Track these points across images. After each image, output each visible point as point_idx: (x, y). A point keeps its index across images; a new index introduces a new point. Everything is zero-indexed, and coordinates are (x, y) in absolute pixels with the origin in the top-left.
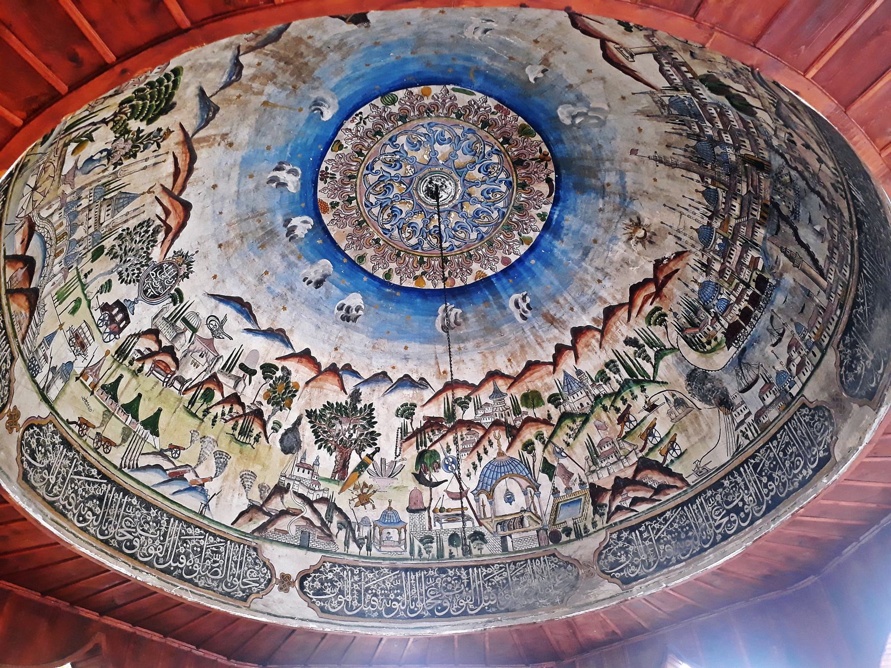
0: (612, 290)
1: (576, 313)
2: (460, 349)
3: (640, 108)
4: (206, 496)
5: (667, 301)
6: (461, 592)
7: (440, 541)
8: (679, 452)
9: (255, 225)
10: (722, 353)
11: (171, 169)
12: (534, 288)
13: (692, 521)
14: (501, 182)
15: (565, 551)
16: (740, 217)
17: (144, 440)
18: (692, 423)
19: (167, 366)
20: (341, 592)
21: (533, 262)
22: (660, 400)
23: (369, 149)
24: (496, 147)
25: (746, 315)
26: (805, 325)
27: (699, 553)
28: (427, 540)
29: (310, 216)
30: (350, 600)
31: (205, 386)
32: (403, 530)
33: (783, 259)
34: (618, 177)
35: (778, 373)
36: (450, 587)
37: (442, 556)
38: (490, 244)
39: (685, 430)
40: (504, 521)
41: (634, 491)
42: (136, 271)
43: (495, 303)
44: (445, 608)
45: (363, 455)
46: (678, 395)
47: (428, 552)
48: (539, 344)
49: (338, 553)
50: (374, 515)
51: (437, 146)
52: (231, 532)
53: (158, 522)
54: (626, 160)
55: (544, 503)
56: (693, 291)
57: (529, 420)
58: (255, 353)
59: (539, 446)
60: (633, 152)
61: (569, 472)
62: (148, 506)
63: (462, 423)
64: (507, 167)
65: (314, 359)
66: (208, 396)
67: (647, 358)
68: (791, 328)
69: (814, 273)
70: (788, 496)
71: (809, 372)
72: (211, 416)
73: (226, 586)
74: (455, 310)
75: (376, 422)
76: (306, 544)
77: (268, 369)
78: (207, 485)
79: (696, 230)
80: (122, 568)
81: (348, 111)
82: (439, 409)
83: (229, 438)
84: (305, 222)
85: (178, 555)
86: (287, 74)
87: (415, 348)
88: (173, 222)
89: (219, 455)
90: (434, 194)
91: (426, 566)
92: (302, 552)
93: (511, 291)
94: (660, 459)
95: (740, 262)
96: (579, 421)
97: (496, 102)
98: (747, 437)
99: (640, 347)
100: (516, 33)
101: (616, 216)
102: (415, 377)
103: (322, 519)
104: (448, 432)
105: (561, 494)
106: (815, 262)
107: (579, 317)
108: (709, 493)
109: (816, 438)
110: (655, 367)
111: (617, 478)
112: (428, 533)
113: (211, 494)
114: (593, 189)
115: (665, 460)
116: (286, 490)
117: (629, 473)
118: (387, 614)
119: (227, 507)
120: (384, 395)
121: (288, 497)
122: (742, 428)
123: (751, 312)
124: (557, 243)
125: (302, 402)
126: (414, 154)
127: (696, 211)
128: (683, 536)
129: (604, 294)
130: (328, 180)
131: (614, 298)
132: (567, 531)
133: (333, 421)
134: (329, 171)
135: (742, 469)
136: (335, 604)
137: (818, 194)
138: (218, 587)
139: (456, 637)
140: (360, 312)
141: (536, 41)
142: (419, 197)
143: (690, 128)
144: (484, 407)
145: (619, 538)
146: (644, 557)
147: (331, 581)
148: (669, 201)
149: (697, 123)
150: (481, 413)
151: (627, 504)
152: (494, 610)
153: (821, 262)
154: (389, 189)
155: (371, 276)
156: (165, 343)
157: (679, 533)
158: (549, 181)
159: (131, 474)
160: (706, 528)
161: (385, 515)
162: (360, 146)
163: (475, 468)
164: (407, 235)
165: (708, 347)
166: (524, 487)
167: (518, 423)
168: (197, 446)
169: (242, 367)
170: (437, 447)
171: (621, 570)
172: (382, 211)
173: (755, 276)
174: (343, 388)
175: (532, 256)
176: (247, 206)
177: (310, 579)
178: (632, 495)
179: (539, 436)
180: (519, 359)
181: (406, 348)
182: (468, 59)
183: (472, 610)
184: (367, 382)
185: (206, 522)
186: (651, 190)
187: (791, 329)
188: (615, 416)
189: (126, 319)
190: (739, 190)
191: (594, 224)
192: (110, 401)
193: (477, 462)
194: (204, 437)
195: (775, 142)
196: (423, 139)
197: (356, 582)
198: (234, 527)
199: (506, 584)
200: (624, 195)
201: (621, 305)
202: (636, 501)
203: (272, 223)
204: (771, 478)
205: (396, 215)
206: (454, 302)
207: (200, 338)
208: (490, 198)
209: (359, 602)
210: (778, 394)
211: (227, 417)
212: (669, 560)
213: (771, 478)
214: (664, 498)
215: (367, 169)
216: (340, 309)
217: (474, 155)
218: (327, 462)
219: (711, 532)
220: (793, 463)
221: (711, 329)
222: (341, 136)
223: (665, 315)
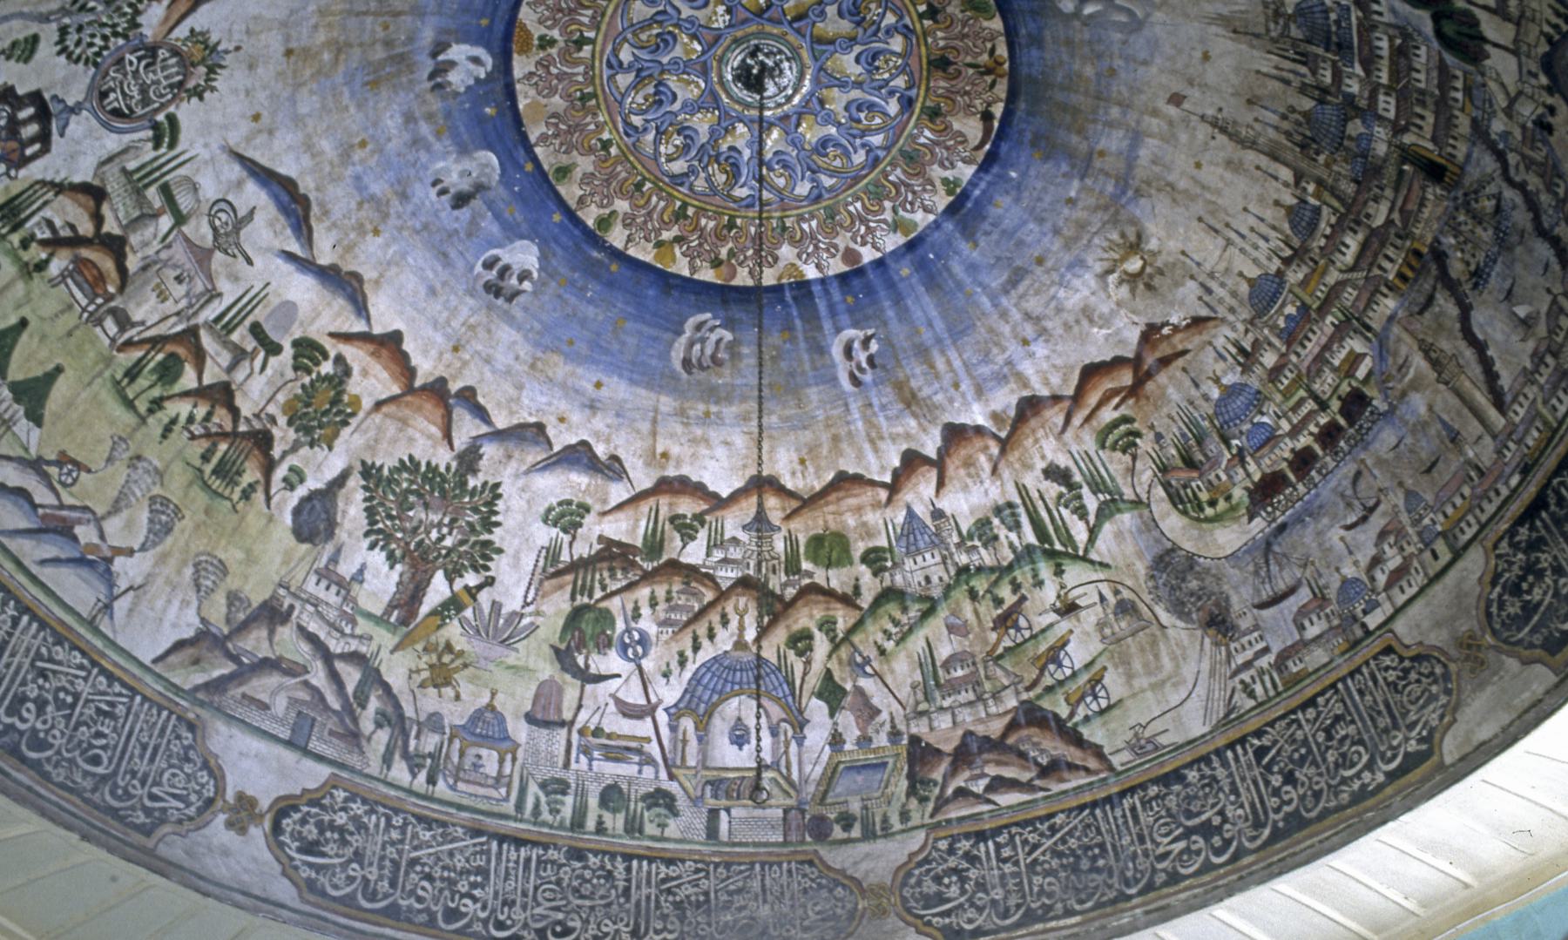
0: (1045, 366)
1: (963, 395)
2: (707, 414)
3: (1225, 11)
5: (1149, 408)
6: (609, 905)
7: (582, 794)
8: (1104, 703)
13: (1108, 839)
14: (891, 93)
15: (837, 858)
16: (1353, 269)
18: (1142, 650)
19: (101, 278)
20: (358, 856)
21: (905, 272)
24: (907, 21)
25: (1303, 461)
26: (1429, 497)
27: (1114, 902)
30: (372, 878)
31: (170, 348)
33: (1419, 362)
34: (1125, 143)
35: (1345, 582)
38: (832, 214)
40: (722, 781)
41: (999, 763)
42: (98, 41)
43: (806, 339)
45: (459, 584)
46: (1126, 594)
47: (554, 812)
48: (872, 442)
49: (368, 776)
50: (455, 715)
52: (149, 679)
54: (1155, 113)
56: (1206, 398)
58: (289, 308)
59: (821, 645)
60: (1176, 99)
63: (674, 566)
64: (915, 66)
65: (405, 357)
66: (169, 371)
67: (1081, 512)
68: (1399, 499)
69: (1481, 399)
70: (1320, 818)
71: (1415, 589)
72: (164, 416)
73: (113, 793)
75: (498, 524)
77: (308, 350)
78: (119, 563)
79: (1250, 281)
83: (190, 474)
84: (476, 60)
85: (21, 699)
87: (618, 389)
89: (159, 504)
90: (753, 80)
92: (289, 756)
93: (844, 319)
94: (1064, 711)
95: (1320, 360)
96: (914, 611)
98: (1252, 695)
99: (1071, 486)
101: (1097, 220)
102: (600, 450)
105: (848, 747)
106: (1491, 377)
107: (966, 404)
108: (1153, 790)
109: (1405, 715)
110: (1093, 533)
112: (560, 774)
113: (123, 584)
114: (1070, 155)
115: (1072, 715)
116: (285, 618)
117: (995, 728)
119: (155, 623)
120: (527, 472)
121: (286, 633)
122: (1246, 676)
123: (1314, 457)
124: (964, 247)
125: (359, 440)
127: (1261, 243)
128: (1085, 864)
129: (1027, 368)
131: (1046, 383)
132: (847, 821)
133: (412, 498)
135: (1229, 754)
136: (340, 878)
138: (94, 790)
140: (527, 285)
142: (721, 77)
143: (1314, 73)
145: (951, 851)
146: (998, 894)
147: (341, 830)
148: (1212, 213)
149: (1334, 63)
150: (718, 555)
151: (979, 787)
153: (1505, 381)
154: (666, 42)
156: (111, 226)
157: (1078, 858)
158: (987, 117)
160: (1134, 857)
161: (477, 716)
163: (682, 663)
164: (671, 150)
165: (1209, 511)
167: (790, 592)
168: (120, 473)
169: (256, 330)
170: (615, 604)
171: (947, 914)
172: (635, 86)
173: (1345, 388)
174: (448, 436)
178: (992, 770)
179: (827, 625)
181: (598, 385)
184: (499, 435)
185: (99, 643)
186: (1183, 184)
187: (1394, 500)
188: (989, 612)
189: (44, 138)
190: (1368, 216)
191: (1048, 225)
193: (689, 653)
194: (139, 458)
195: (1498, 126)
197: (393, 843)
198: (158, 669)
200: (1127, 185)
201: (1056, 399)
202: (999, 784)
204: (1290, 779)
205: (660, 103)
206: (722, 313)
207: (187, 240)
209: (393, 884)
210: (1336, 622)
211: (197, 429)
212: (1049, 908)
213: (1290, 779)
214: (1056, 788)
216: (488, 265)
217: (858, 24)
218: (382, 580)
220: (1343, 755)
221: (1224, 477)
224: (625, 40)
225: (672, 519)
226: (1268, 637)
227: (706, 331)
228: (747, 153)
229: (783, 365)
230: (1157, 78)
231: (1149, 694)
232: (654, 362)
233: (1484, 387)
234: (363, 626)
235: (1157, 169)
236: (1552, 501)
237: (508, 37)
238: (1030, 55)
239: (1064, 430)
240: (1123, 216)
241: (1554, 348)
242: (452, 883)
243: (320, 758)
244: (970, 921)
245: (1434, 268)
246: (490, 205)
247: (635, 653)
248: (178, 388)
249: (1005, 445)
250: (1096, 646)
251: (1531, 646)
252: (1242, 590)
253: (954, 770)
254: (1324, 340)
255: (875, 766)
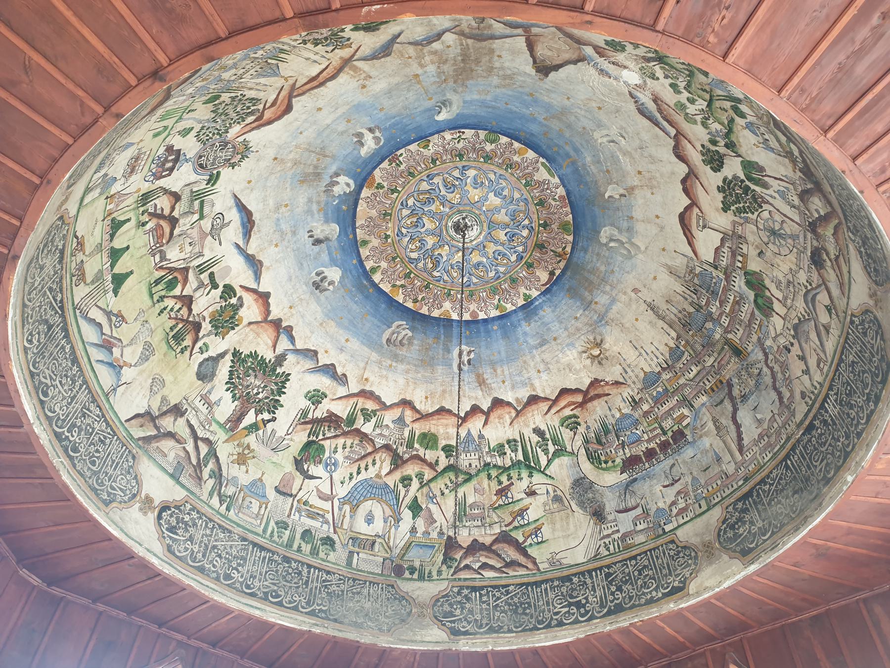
2: (391, 366)
3: (669, 264)
4: (119, 380)
7: (294, 531)
9: (313, 160)
10: (614, 474)
11: (314, 74)
12: (483, 349)
13: (532, 601)
14: (515, 252)
16: (691, 380)
17: (106, 292)
18: (562, 520)
19: (163, 235)
20: (191, 539)
21: (495, 328)
22: (541, 490)
23: (443, 162)
24: (533, 225)
25: (650, 454)
28: (282, 525)
29: (355, 182)
30: (196, 550)
31: (175, 274)
32: (264, 506)
33: (710, 425)
36: (289, 578)
37: (291, 546)
39: (553, 523)
41: (486, 557)
42: (211, 135)
43: (444, 344)
44: (280, 596)
45: (260, 417)
46: (559, 493)
49: (201, 500)
51: (491, 195)
52: (121, 429)
53: (74, 382)
54: (625, 293)
55: (400, 536)
56: (613, 416)
57: (417, 457)
58: (228, 269)
59: (415, 484)
60: (636, 291)
61: (433, 518)
62: (75, 361)
63: (358, 431)
66: (171, 285)
67: (546, 451)
68: (689, 479)
69: (734, 447)
70: (631, 608)
71: (689, 518)
72: (162, 305)
74: (408, 331)
75: (284, 393)
76: (177, 475)
77: (229, 290)
79: (645, 372)
80: (28, 406)
81: (456, 125)
82: (345, 409)
83: (163, 335)
84: (348, 185)
85: (74, 425)
86: (453, 68)
87: (355, 344)
88: (268, 115)
89: (148, 347)
91: (273, 549)
92: (171, 482)
94: (521, 539)
95: (668, 413)
97: (564, 193)
98: (608, 549)
99: (544, 439)
100: (631, 157)
102: (340, 371)
103: (199, 459)
104: (342, 434)
105: (418, 535)
106: (740, 438)
108: (556, 583)
110: (549, 462)
111: (475, 540)
114: (582, 299)
115: (525, 541)
117: (488, 540)
118: (225, 579)
119: (129, 403)
121: (181, 421)
122: (607, 541)
123: (656, 453)
124: (523, 323)
126: (470, 189)
127: (655, 359)
128: (520, 610)
130: (394, 164)
131: (544, 391)
132: (412, 570)
133: (250, 371)
134: (401, 158)
137: (779, 394)
138: (90, 478)
139: (276, 627)
140: (331, 288)
141: (640, 173)
144: (384, 428)
145: (459, 593)
146: (478, 617)
147: (186, 524)
149: (708, 298)
150: (378, 431)
151: (476, 566)
152: (323, 615)
153: (746, 442)
155: (361, 262)
156: (176, 214)
158: (552, 273)
159: (79, 318)
160: (544, 611)
161: (253, 483)
162: (439, 156)
163: (351, 479)
164: (414, 247)
166: (387, 515)
167: (406, 456)
170: (326, 444)
171: (453, 622)
173: (675, 428)
174: (274, 347)
175: (497, 323)
176: (323, 141)
177: (169, 512)
178: (483, 560)
179: (420, 476)
180: (436, 401)
181: (347, 340)
182: (576, 150)
183: (303, 607)
184: (297, 351)
186: (627, 325)
189: (171, 170)
192: (107, 237)
193: (355, 474)
195: (769, 343)
196: (487, 183)
197: (207, 536)
198: (126, 425)
199: (340, 596)
200: (603, 318)
201: (546, 399)
203: (325, 168)
206: (410, 323)
207: (201, 227)
208: (497, 259)
209: (204, 556)
210: (651, 525)
211: (173, 315)
212: (502, 627)
213: (619, 589)
214: (512, 573)
215: (428, 176)
216: (318, 274)
219: (548, 615)
222: (435, 139)
223: (579, 424)
224: (413, 196)
225: (362, 410)
226: (619, 525)
227: (402, 329)
228: (445, 258)
229: (430, 353)
230: (631, 280)
231: (561, 539)
232: (374, 337)
233: (736, 443)
234: (214, 427)
235: (619, 316)
236: (755, 494)
237: (365, 180)
238: (580, 254)
239: (546, 413)
240: (597, 331)
241: (769, 434)
242: (230, 561)
243: (183, 486)
244: (464, 627)
245: (726, 390)
246: (329, 248)
247: (331, 469)
248: (172, 294)
249: (518, 413)
250: (540, 513)
251: (735, 551)
252: (612, 503)
253: (465, 556)
254: (672, 406)
255: (431, 547)
